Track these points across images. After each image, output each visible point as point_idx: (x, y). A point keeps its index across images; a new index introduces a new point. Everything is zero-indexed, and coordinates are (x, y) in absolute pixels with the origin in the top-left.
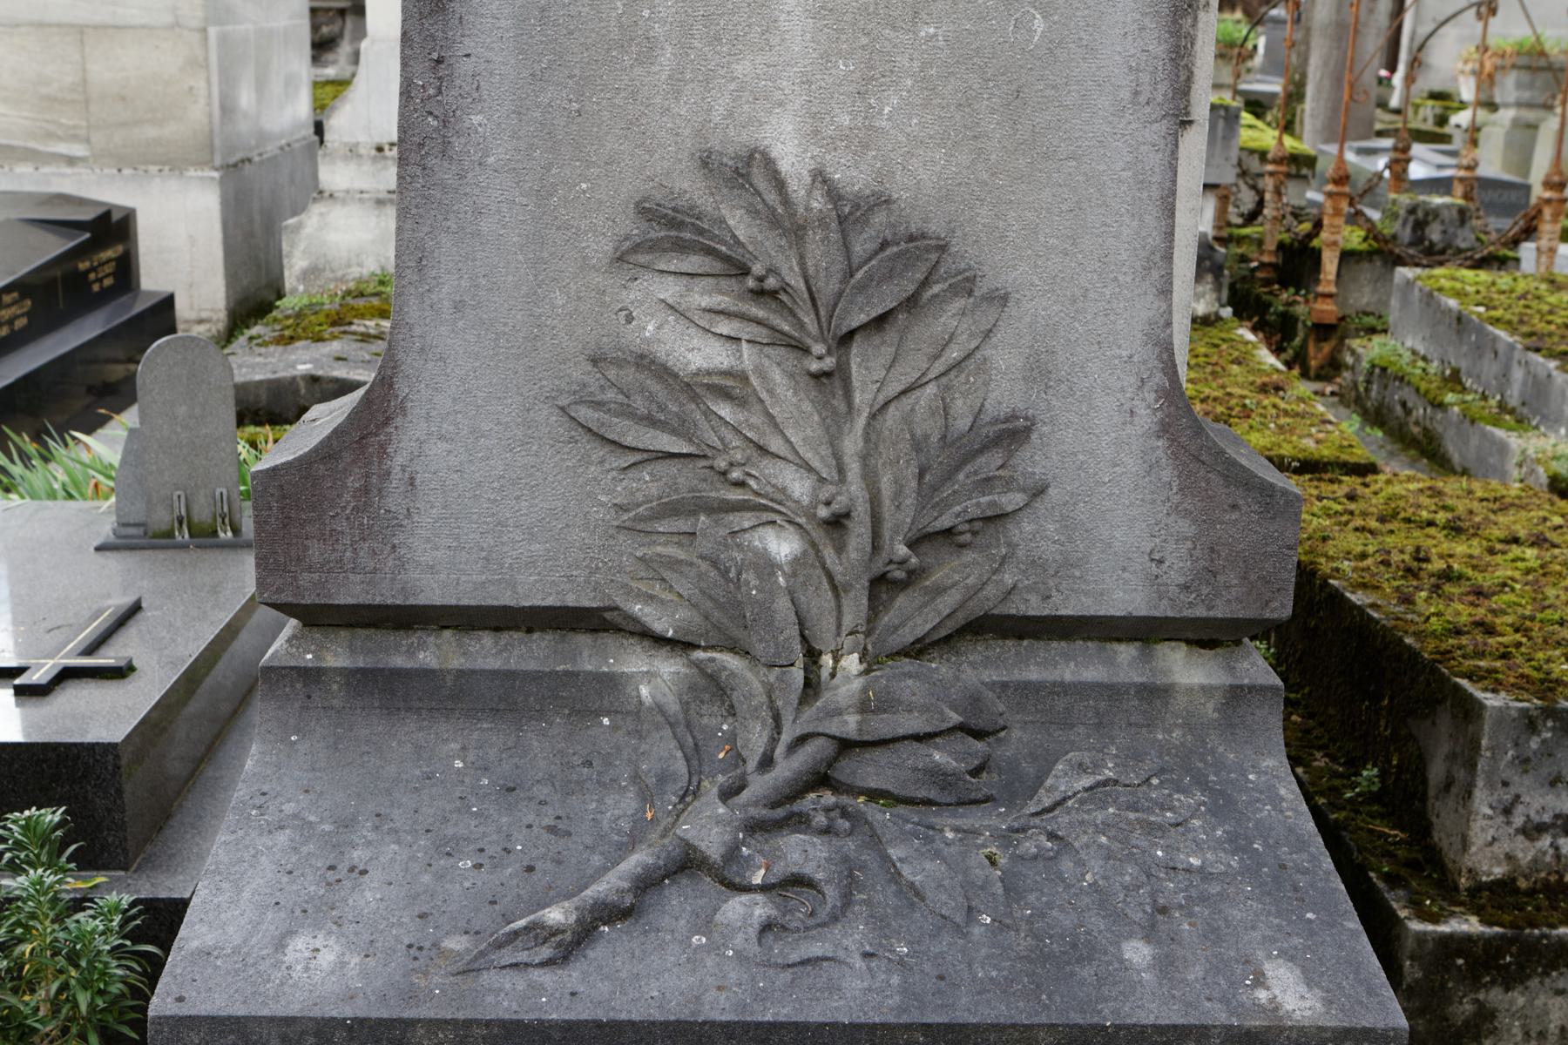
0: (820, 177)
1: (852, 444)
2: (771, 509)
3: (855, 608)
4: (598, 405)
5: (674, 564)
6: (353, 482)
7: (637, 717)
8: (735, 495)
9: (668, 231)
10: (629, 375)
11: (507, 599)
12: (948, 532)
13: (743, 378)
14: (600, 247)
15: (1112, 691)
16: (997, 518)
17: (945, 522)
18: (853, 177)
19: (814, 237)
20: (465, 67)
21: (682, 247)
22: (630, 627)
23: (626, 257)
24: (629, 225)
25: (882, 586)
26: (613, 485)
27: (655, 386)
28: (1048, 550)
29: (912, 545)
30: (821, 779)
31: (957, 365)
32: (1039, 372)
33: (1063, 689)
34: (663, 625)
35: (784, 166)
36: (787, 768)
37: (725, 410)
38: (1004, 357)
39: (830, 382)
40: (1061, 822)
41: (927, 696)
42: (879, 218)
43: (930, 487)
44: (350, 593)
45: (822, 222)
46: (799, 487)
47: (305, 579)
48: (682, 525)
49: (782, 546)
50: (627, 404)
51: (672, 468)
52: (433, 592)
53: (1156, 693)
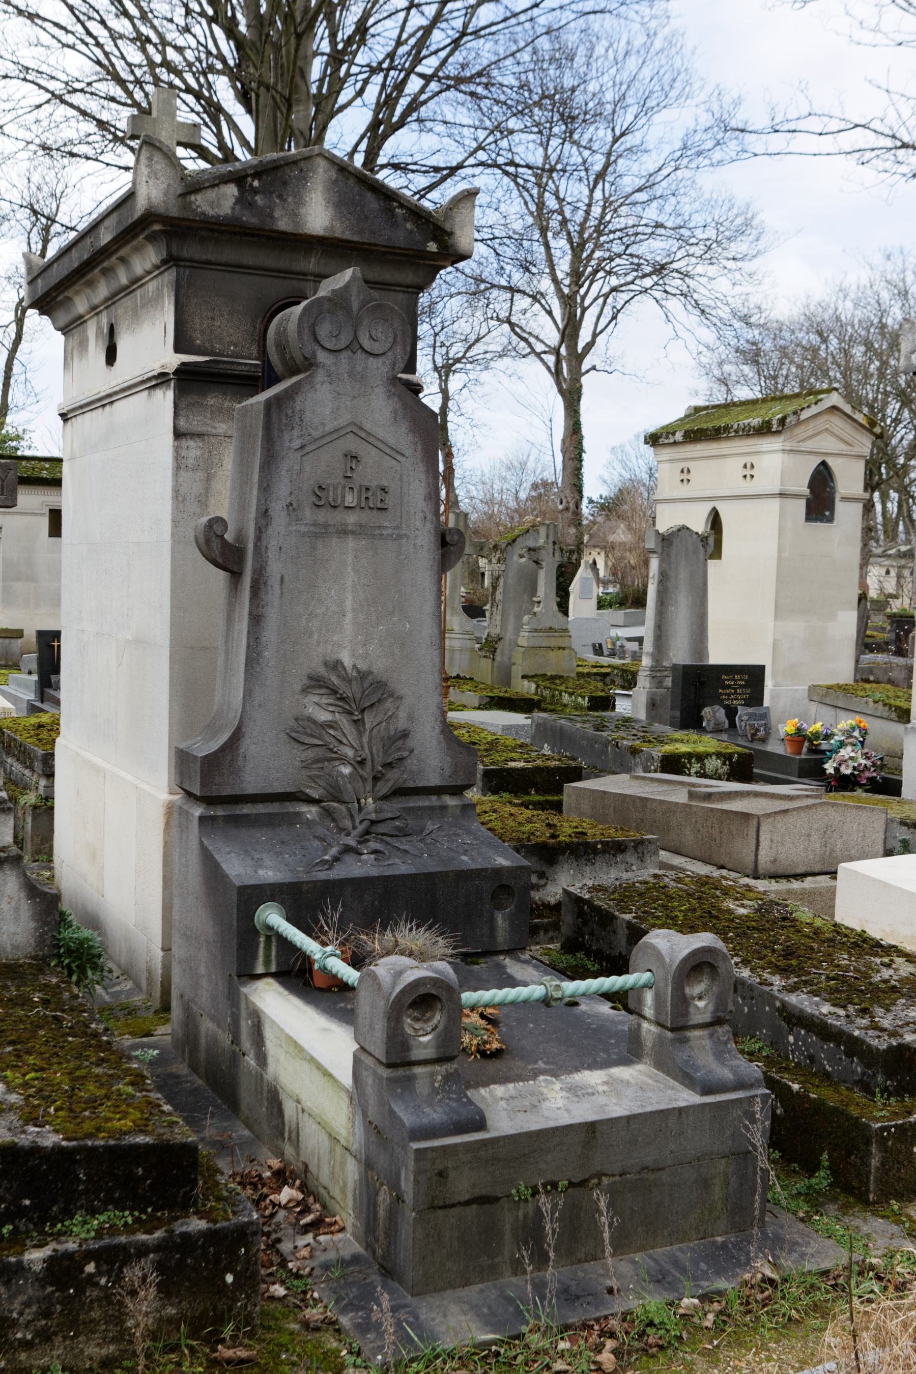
0: (354, 667)
1: (365, 740)
2: (343, 760)
3: (369, 787)
4: (297, 732)
5: (318, 776)
6: (229, 758)
7: (309, 824)
8: (335, 756)
9: (316, 683)
10: (306, 723)
11: (270, 791)
12: (390, 764)
13: (336, 722)
14: (297, 688)
15: (432, 808)
16: (401, 759)
17: (390, 760)
18: (363, 666)
19: (354, 682)
20: (265, 639)
21: (320, 687)
22: (304, 798)
23: (305, 690)
24: (306, 681)
25: (376, 779)
26: (301, 754)
27: (313, 726)
28: (415, 768)
29: (384, 766)
30: (367, 832)
31: (390, 717)
32: (411, 718)
33: (420, 808)
34: (315, 795)
35: (346, 664)
36: (361, 828)
37: (332, 732)
38: (402, 714)
39: (358, 723)
40: (433, 835)
41: (392, 808)
42: (370, 677)
43: (386, 749)
44: (226, 791)
45: (356, 679)
46: (350, 753)
47: (214, 788)
48: (320, 765)
49: (346, 770)
50: (302, 732)
51: (317, 749)
52: (250, 790)
53: (444, 808)
